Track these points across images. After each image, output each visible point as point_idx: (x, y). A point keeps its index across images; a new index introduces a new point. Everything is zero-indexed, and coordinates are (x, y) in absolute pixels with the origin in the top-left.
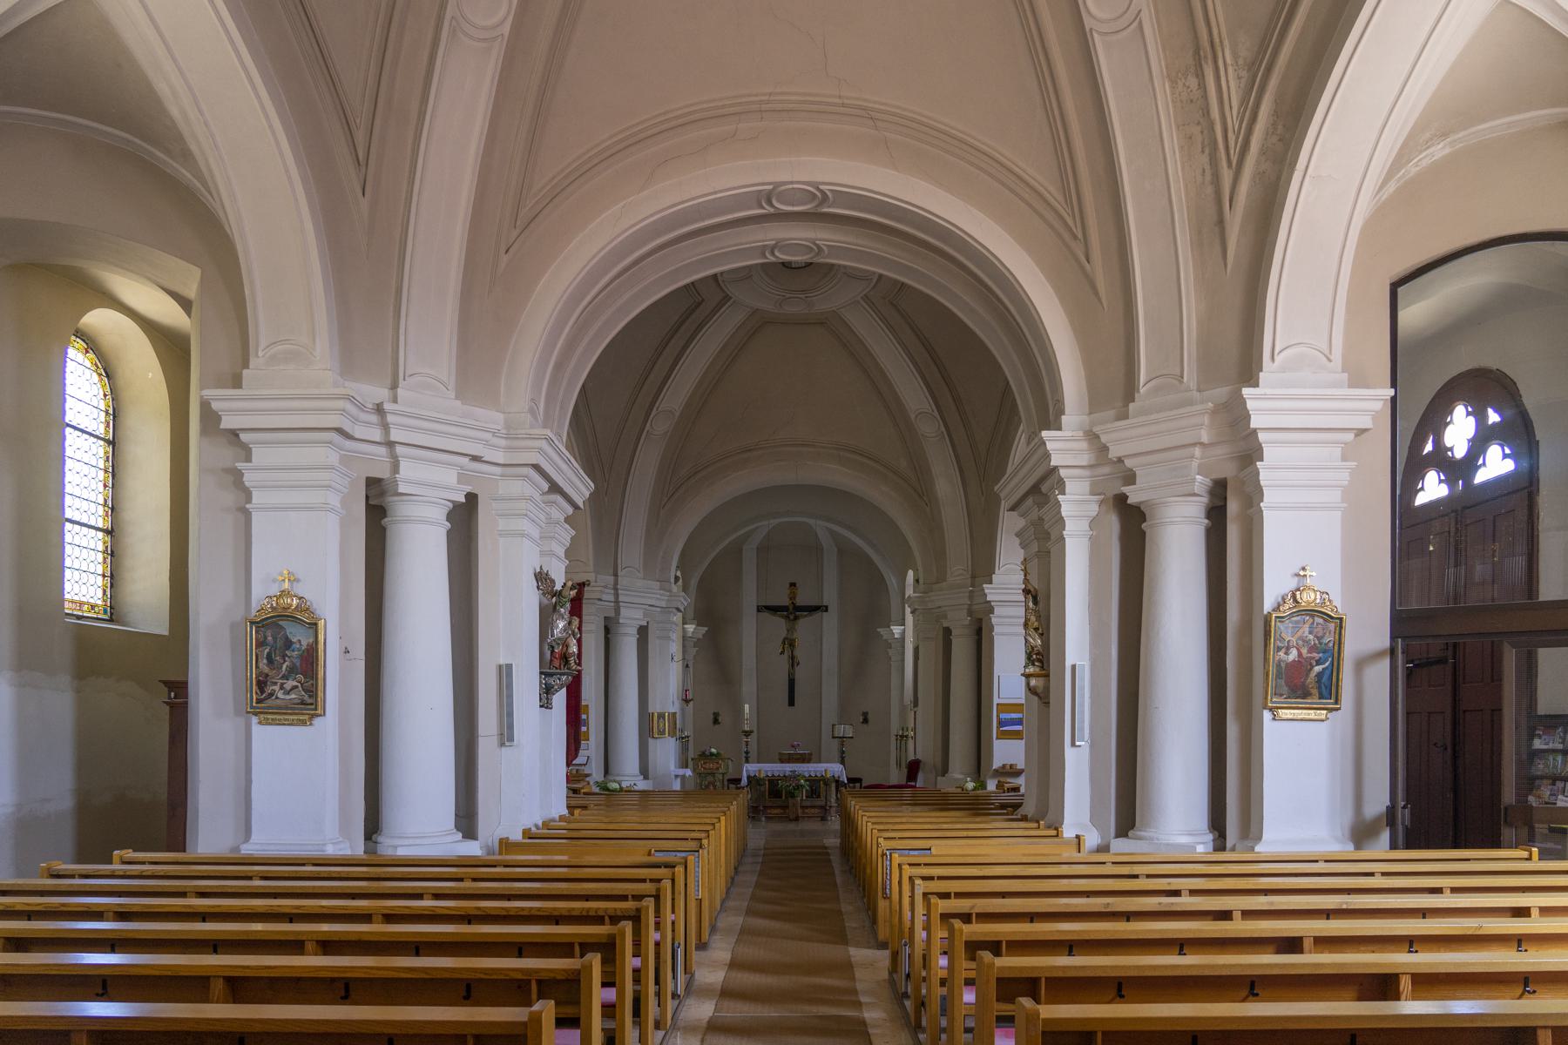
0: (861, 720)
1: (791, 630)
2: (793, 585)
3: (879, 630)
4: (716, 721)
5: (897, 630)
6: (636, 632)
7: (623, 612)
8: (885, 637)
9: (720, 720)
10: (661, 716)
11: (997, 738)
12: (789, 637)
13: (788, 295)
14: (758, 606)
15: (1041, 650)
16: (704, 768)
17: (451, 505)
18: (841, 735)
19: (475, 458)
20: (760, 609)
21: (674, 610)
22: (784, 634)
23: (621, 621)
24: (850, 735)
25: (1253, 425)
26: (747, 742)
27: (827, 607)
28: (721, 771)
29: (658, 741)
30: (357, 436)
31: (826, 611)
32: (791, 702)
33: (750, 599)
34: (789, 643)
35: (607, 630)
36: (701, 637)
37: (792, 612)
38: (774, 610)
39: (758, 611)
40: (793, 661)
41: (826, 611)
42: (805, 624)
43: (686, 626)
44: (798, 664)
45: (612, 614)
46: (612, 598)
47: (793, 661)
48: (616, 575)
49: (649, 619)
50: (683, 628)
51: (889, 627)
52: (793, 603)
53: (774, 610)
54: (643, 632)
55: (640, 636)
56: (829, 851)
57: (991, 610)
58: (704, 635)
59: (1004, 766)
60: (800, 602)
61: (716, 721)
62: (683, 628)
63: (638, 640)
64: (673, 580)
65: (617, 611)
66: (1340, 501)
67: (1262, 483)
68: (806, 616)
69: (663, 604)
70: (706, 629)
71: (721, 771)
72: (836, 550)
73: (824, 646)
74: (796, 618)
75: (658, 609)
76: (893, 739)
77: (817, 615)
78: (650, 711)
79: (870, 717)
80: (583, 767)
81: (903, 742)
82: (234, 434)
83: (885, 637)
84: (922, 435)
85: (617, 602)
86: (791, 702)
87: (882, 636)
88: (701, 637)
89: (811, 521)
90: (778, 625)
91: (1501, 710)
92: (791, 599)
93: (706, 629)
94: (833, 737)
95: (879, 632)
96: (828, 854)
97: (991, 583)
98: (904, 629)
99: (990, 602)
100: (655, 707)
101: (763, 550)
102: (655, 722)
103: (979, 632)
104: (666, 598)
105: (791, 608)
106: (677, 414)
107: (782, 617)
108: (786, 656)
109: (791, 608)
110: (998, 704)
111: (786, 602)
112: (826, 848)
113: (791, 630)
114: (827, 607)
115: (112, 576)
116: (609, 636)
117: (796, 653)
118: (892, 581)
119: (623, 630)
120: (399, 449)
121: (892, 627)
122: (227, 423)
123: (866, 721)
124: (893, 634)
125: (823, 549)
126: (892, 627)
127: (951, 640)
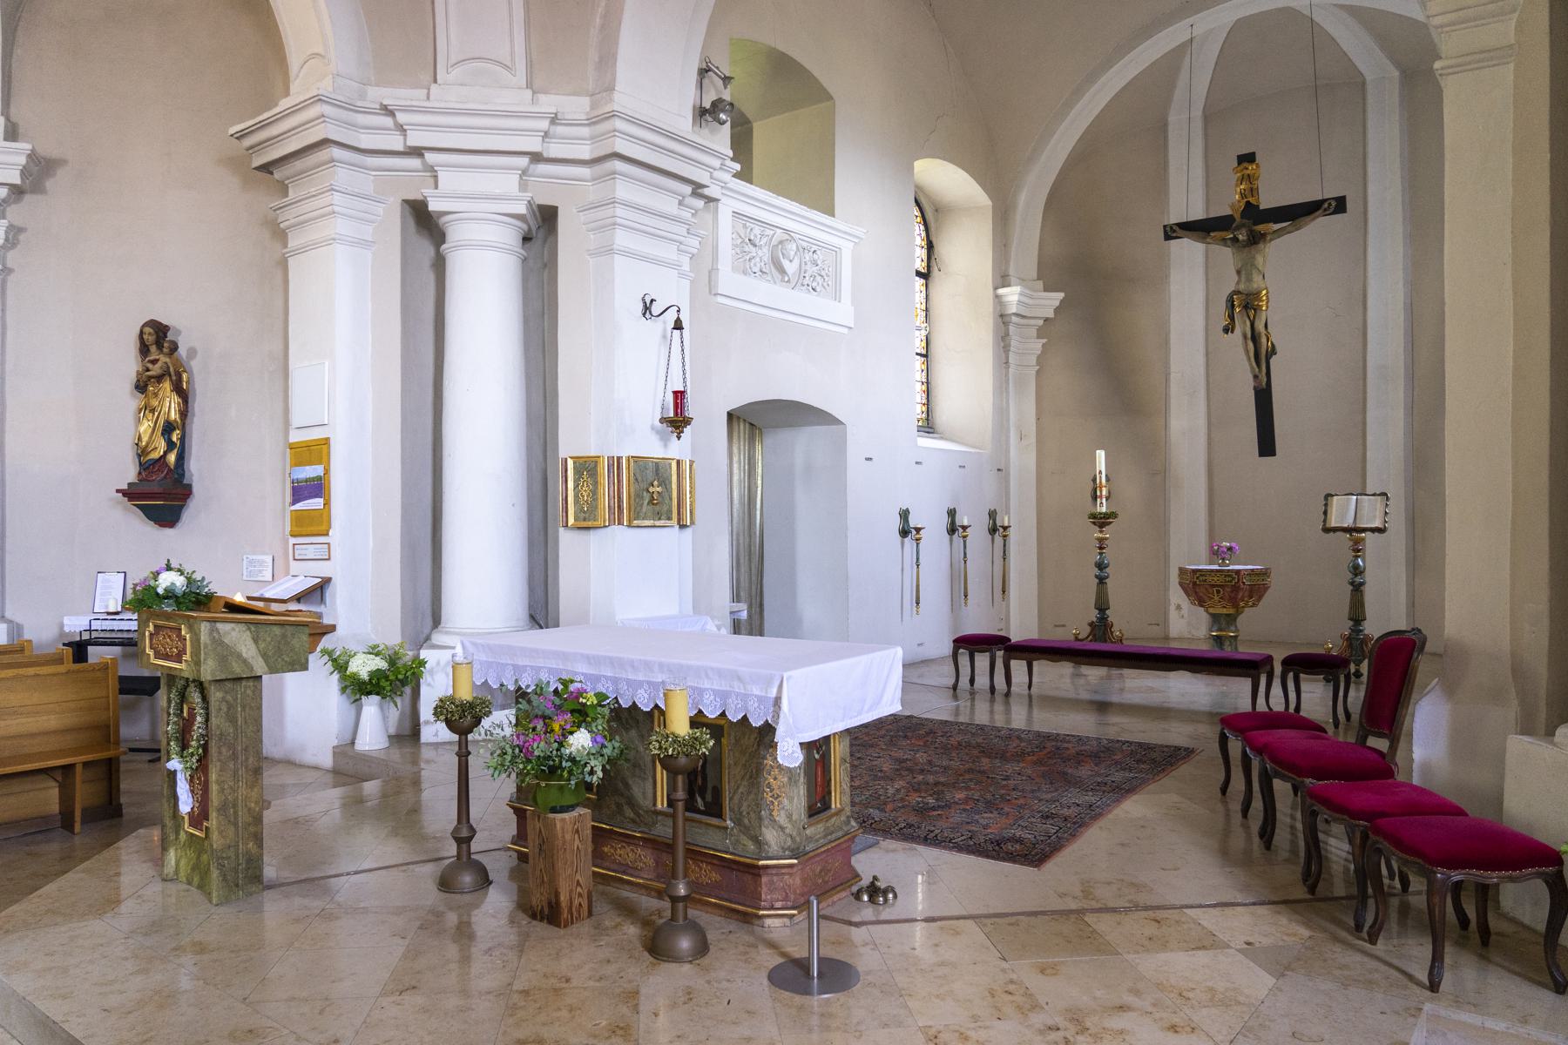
2: (1248, 158)
10: (587, 467)
12: (1242, 287)
18: (1348, 522)
24: (1377, 524)
26: (1101, 540)
32: (1267, 446)
34: (1244, 304)
36: (1051, 314)
40: (1262, 355)
43: (1001, 291)
47: (1262, 355)
50: (997, 297)
58: (1057, 310)
60: (1266, 201)
62: (997, 297)
66: (821, 955)
68: (1279, 233)
70: (1061, 295)
72: (1397, 74)
73: (1371, 314)
86: (1267, 446)
88: (1051, 314)
93: (1061, 295)
94: (1327, 530)
107: (1224, 241)
115: (928, 383)
125: (1364, 84)
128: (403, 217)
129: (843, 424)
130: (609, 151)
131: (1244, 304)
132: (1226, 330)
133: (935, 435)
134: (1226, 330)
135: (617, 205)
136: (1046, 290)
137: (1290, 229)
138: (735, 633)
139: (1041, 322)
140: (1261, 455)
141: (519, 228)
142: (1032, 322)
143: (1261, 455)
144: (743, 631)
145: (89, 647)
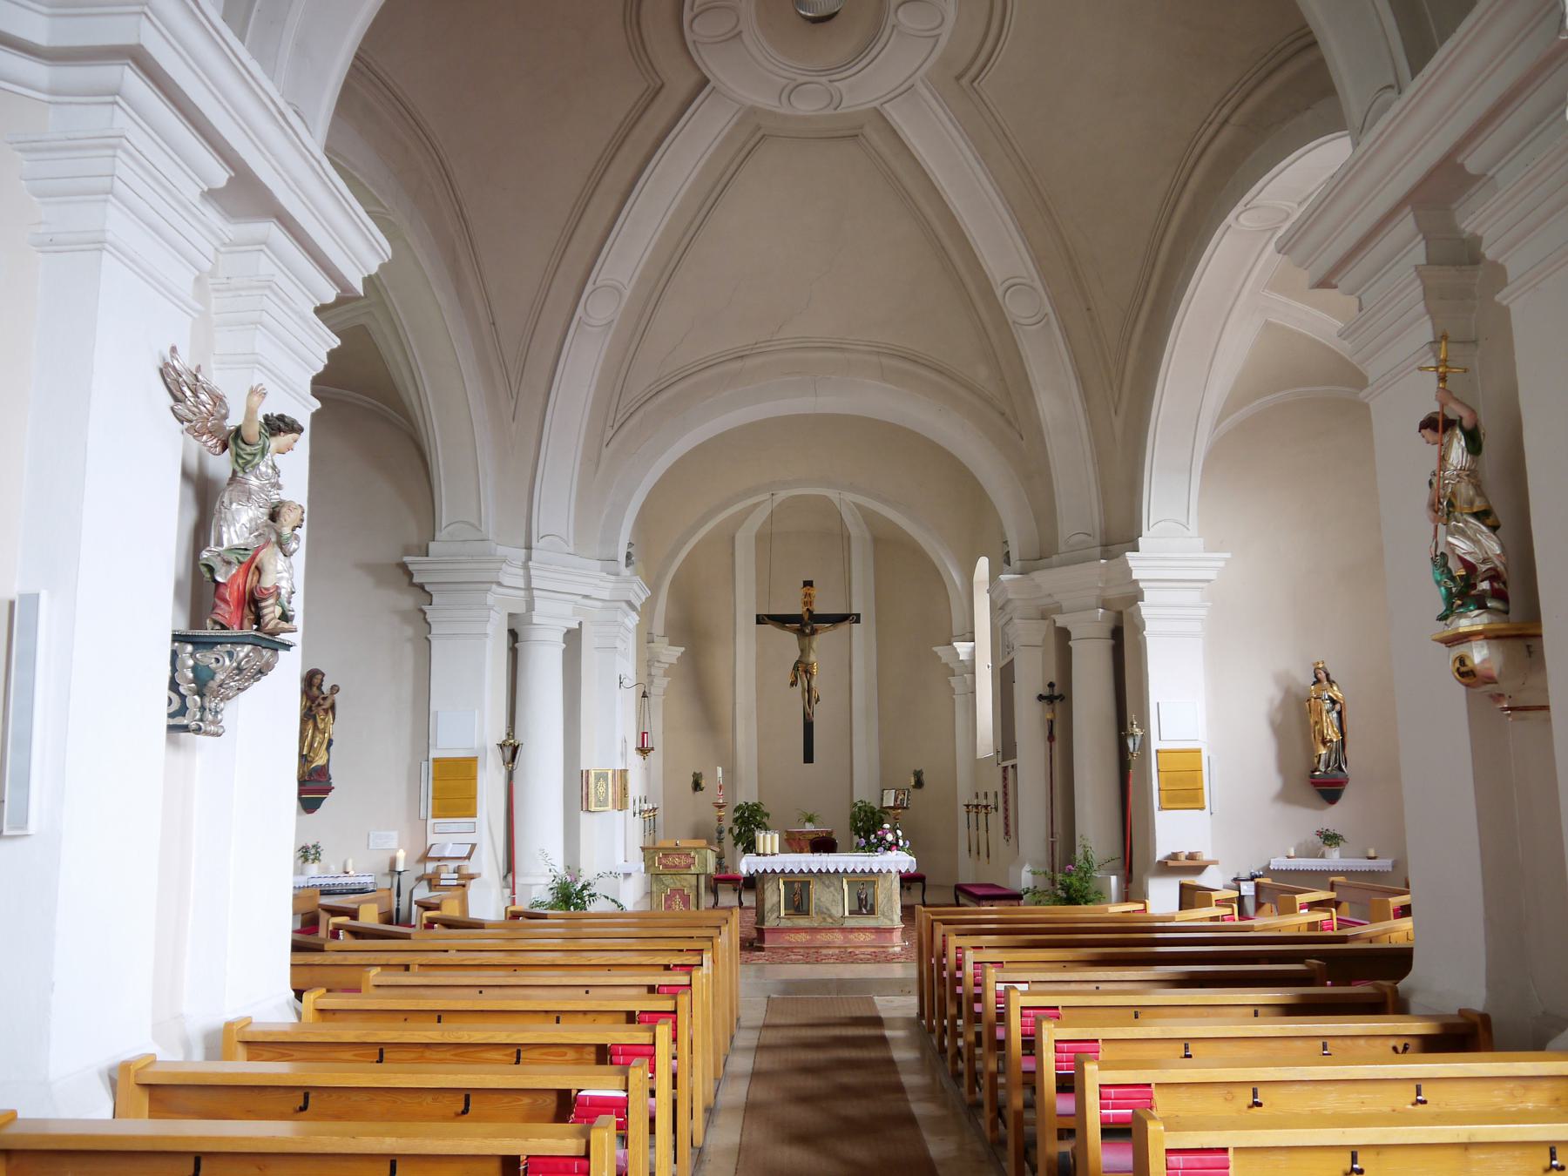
0: (913, 783)
1: (804, 651)
2: (808, 584)
3: (935, 649)
4: (697, 786)
5: (962, 648)
6: (561, 640)
7: (539, 604)
8: (943, 661)
9: (703, 784)
10: (601, 776)
11: (1161, 809)
13: (801, 79)
14: (757, 616)
15: (1501, 568)
16: (666, 866)
17: (566, 630)
19: (586, 597)
20: (760, 620)
21: (624, 605)
22: (795, 655)
23: (535, 620)
25: (1134, 577)
27: (858, 616)
28: (693, 870)
29: (595, 816)
30: (506, 584)
31: (858, 621)
33: (746, 606)
34: (802, 669)
35: (513, 635)
37: (804, 624)
38: (781, 620)
39: (758, 622)
41: (858, 621)
42: (824, 642)
44: (818, 700)
45: (520, 609)
46: (521, 583)
48: (529, 547)
49: (581, 619)
51: (950, 644)
52: (808, 609)
53: (781, 620)
54: (573, 638)
55: (567, 645)
56: (888, 1033)
57: (1137, 596)
59: (1174, 856)
60: (819, 609)
61: (697, 786)
63: (564, 651)
64: (622, 558)
65: (530, 606)
67: (1143, 616)
69: (606, 595)
71: (693, 870)
74: (814, 632)
75: (599, 604)
76: (962, 811)
77: (843, 627)
78: (584, 767)
79: (925, 778)
80: (466, 862)
81: (982, 816)
82: (421, 587)
83: (943, 661)
84: (1014, 322)
85: (529, 588)
86: (808, 757)
87: (940, 658)
88: (675, 661)
89: (831, 494)
90: (787, 640)
91: (1202, 789)
92: (805, 603)
93: (683, 649)
95: (936, 653)
96: (883, 1041)
97: (1137, 550)
98: (974, 648)
99: (1136, 582)
100: (591, 761)
101: (765, 540)
102: (592, 786)
103: (1117, 634)
104: (611, 585)
105: (806, 617)
106: (627, 293)
108: (798, 688)
109: (806, 617)
110: (1157, 751)
111: (797, 609)
112: (877, 1022)
113: (804, 651)
114: (858, 616)
116: (517, 645)
117: (813, 684)
118: (955, 576)
119: (537, 634)
120: (535, 592)
121: (954, 644)
122: (416, 580)
123: (919, 784)
124: (958, 654)
125: (849, 538)
126: (954, 644)
127: (1070, 649)
128: (298, 807)
129: (1413, 79)
130: (122, 134)
131: (802, 669)
132: (792, 685)
133: (300, 861)
134: (792, 685)
135: (119, 152)
136: (671, 644)
137: (832, 628)
138: (174, 635)
139: (667, 666)
140: (805, 762)
141: (398, 910)
142: (662, 665)
143: (805, 762)
144: (619, 1131)
145: (978, 757)
